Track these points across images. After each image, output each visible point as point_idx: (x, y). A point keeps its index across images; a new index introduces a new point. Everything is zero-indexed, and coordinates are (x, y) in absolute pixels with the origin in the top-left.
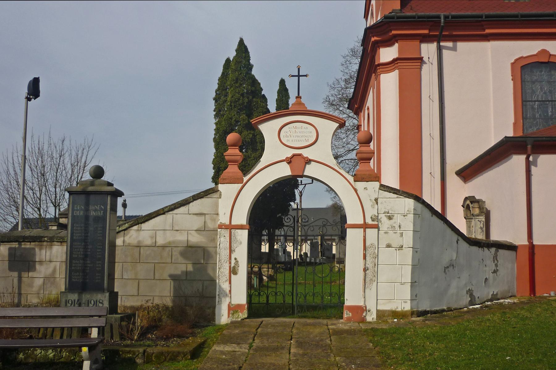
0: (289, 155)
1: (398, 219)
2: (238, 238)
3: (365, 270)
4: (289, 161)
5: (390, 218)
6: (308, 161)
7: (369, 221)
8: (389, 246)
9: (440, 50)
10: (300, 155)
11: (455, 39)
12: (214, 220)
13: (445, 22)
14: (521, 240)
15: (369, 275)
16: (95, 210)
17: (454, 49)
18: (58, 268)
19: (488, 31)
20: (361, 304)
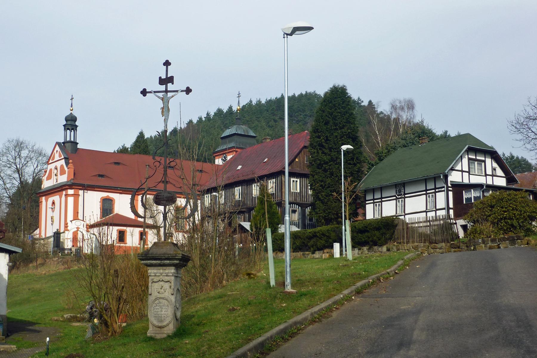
11: (87, 190)
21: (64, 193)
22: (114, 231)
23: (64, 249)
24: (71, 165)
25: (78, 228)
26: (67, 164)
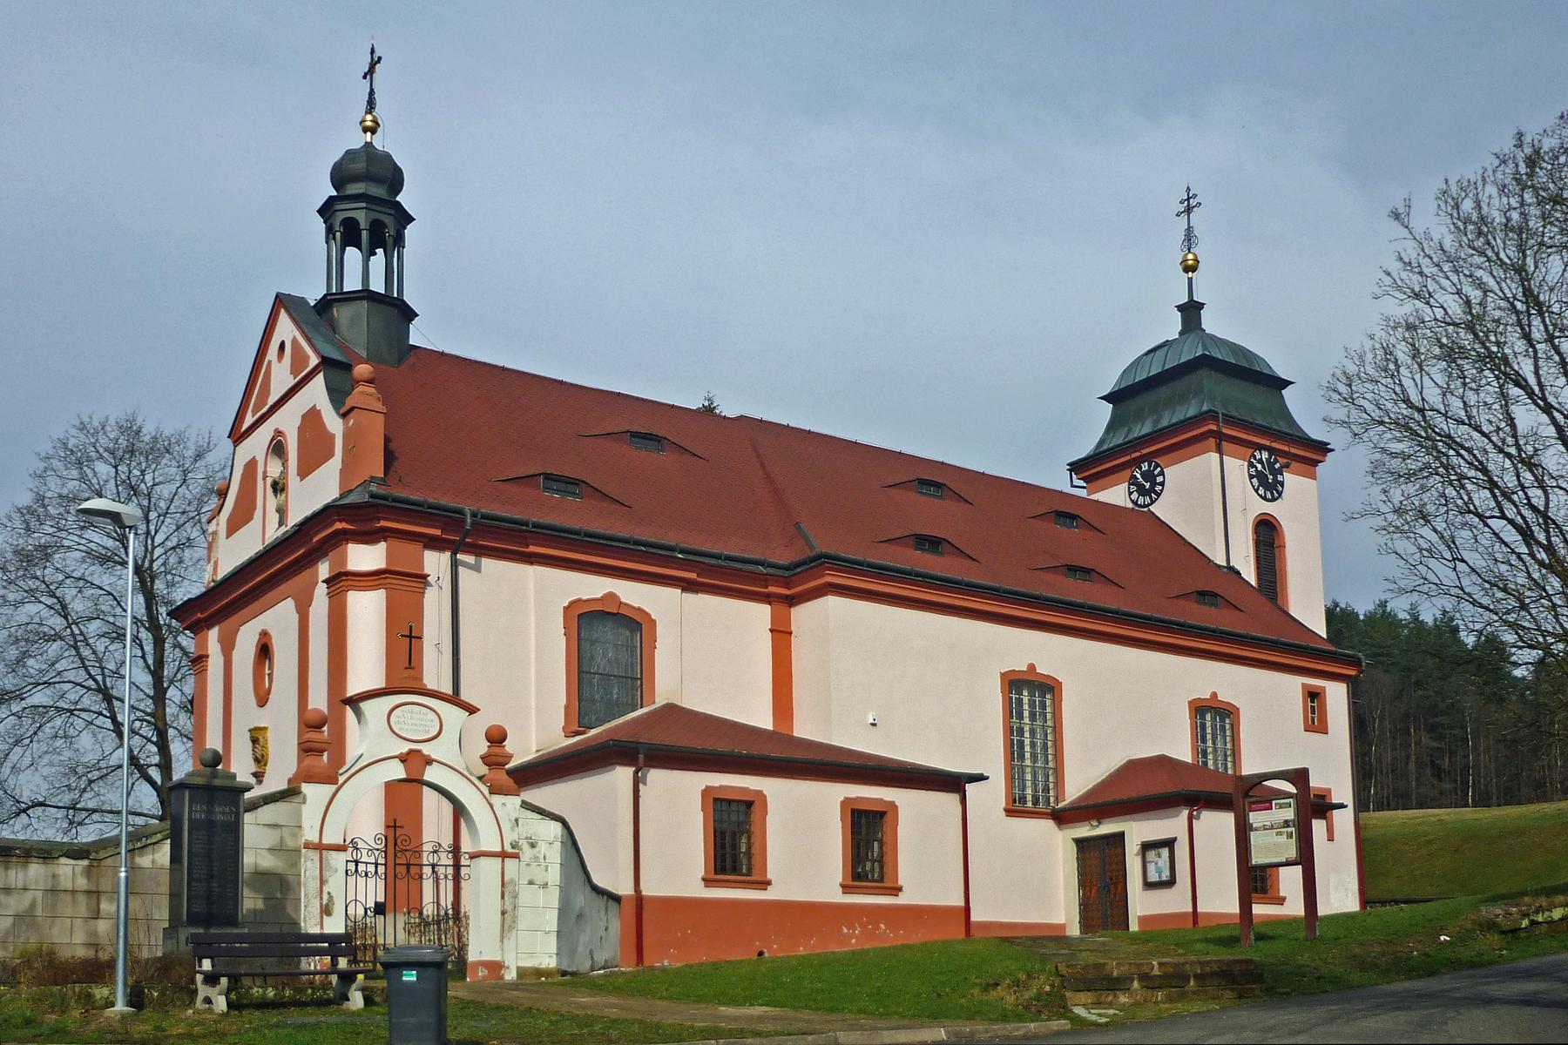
0: (405, 750)
1: (542, 848)
2: (333, 863)
3: (503, 913)
4: (404, 759)
5: (533, 846)
6: (429, 761)
7: (508, 849)
8: (531, 883)
9: (455, 565)
10: (419, 751)
11: (480, 551)
12: (295, 836)
13: (473, 524)
14: (625, 888)
15: (507, 920)
16: (224, 813)
17: (477, 568)
18: (39, 900)
19: (532, 549)
20: (498, 958)
21: (324, 570)
22: (679, 798)
23: (296, 943)
24: (363, 395)
25: (415, 760)
26: (337, 395)
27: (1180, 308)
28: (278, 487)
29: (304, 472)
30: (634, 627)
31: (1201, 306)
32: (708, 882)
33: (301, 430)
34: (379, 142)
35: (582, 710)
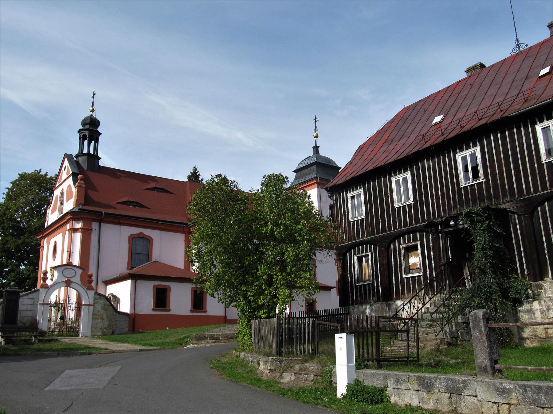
6: (72, 282)
27: (313, 147)
28: (62, 203)
29: (67, 201)
30: (149, 241)
31: (319, 147)
32: (153, 310)
33: (67, 189)
34: (94, 115)
35: (131, 263)
